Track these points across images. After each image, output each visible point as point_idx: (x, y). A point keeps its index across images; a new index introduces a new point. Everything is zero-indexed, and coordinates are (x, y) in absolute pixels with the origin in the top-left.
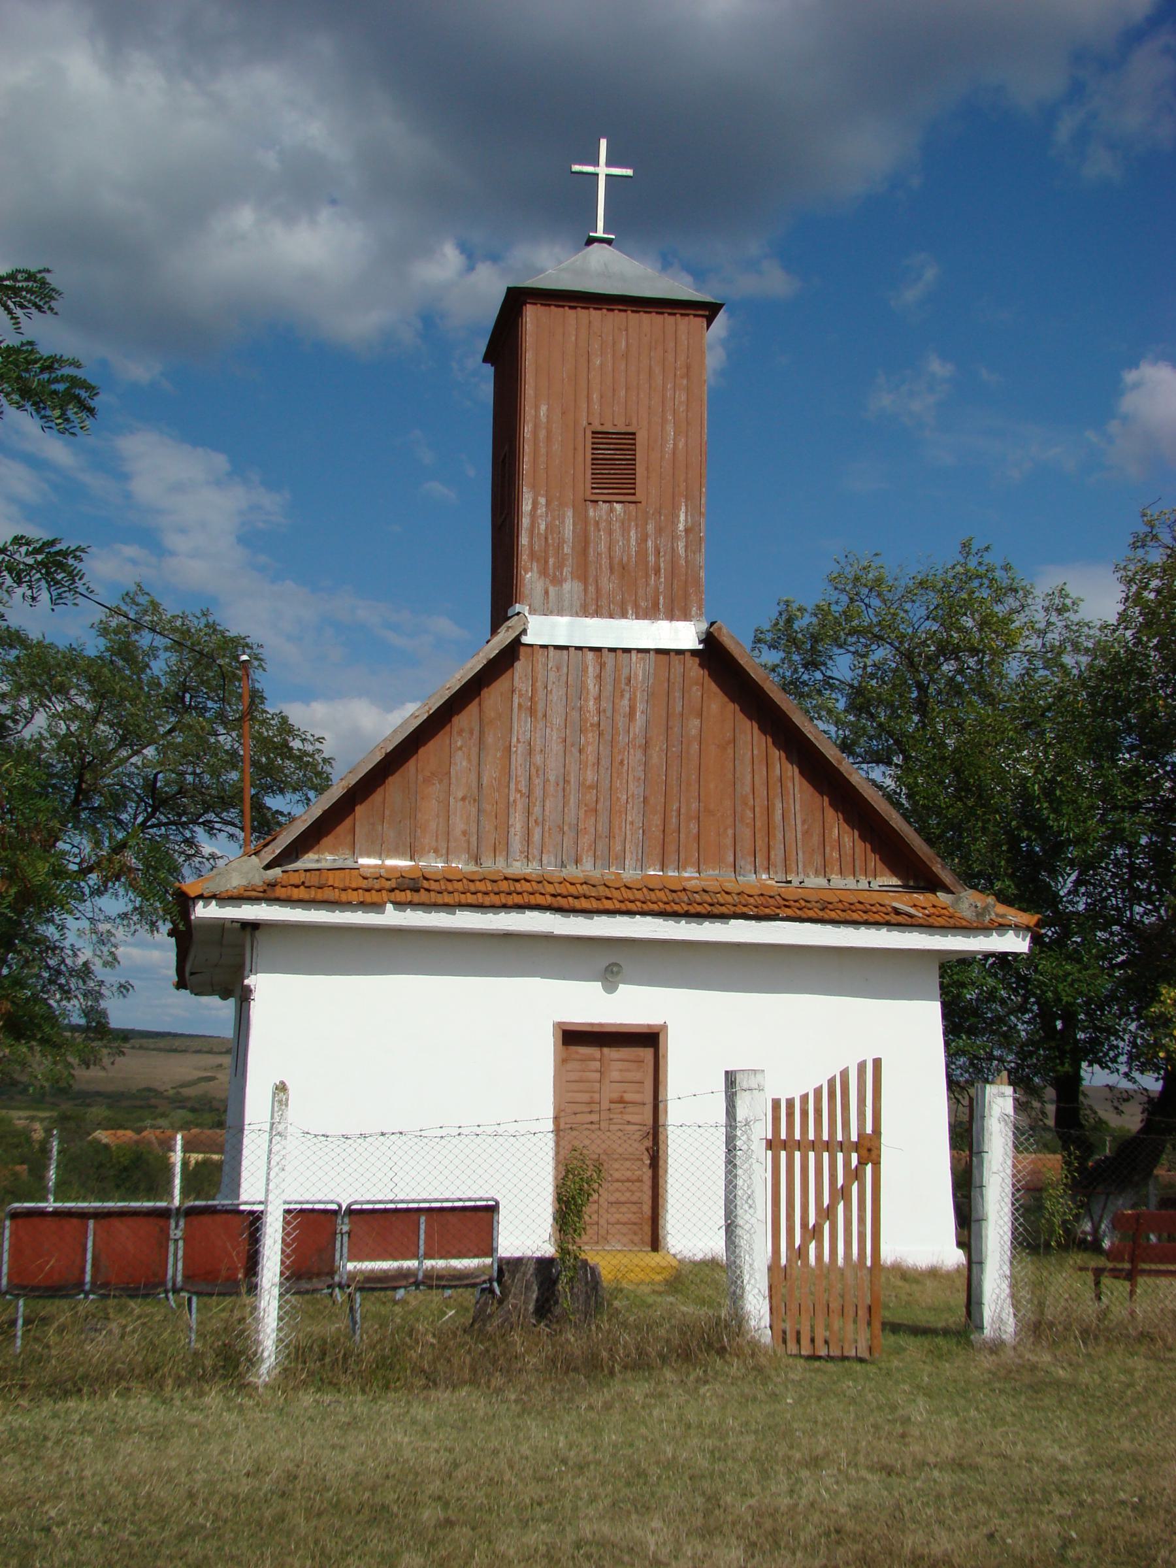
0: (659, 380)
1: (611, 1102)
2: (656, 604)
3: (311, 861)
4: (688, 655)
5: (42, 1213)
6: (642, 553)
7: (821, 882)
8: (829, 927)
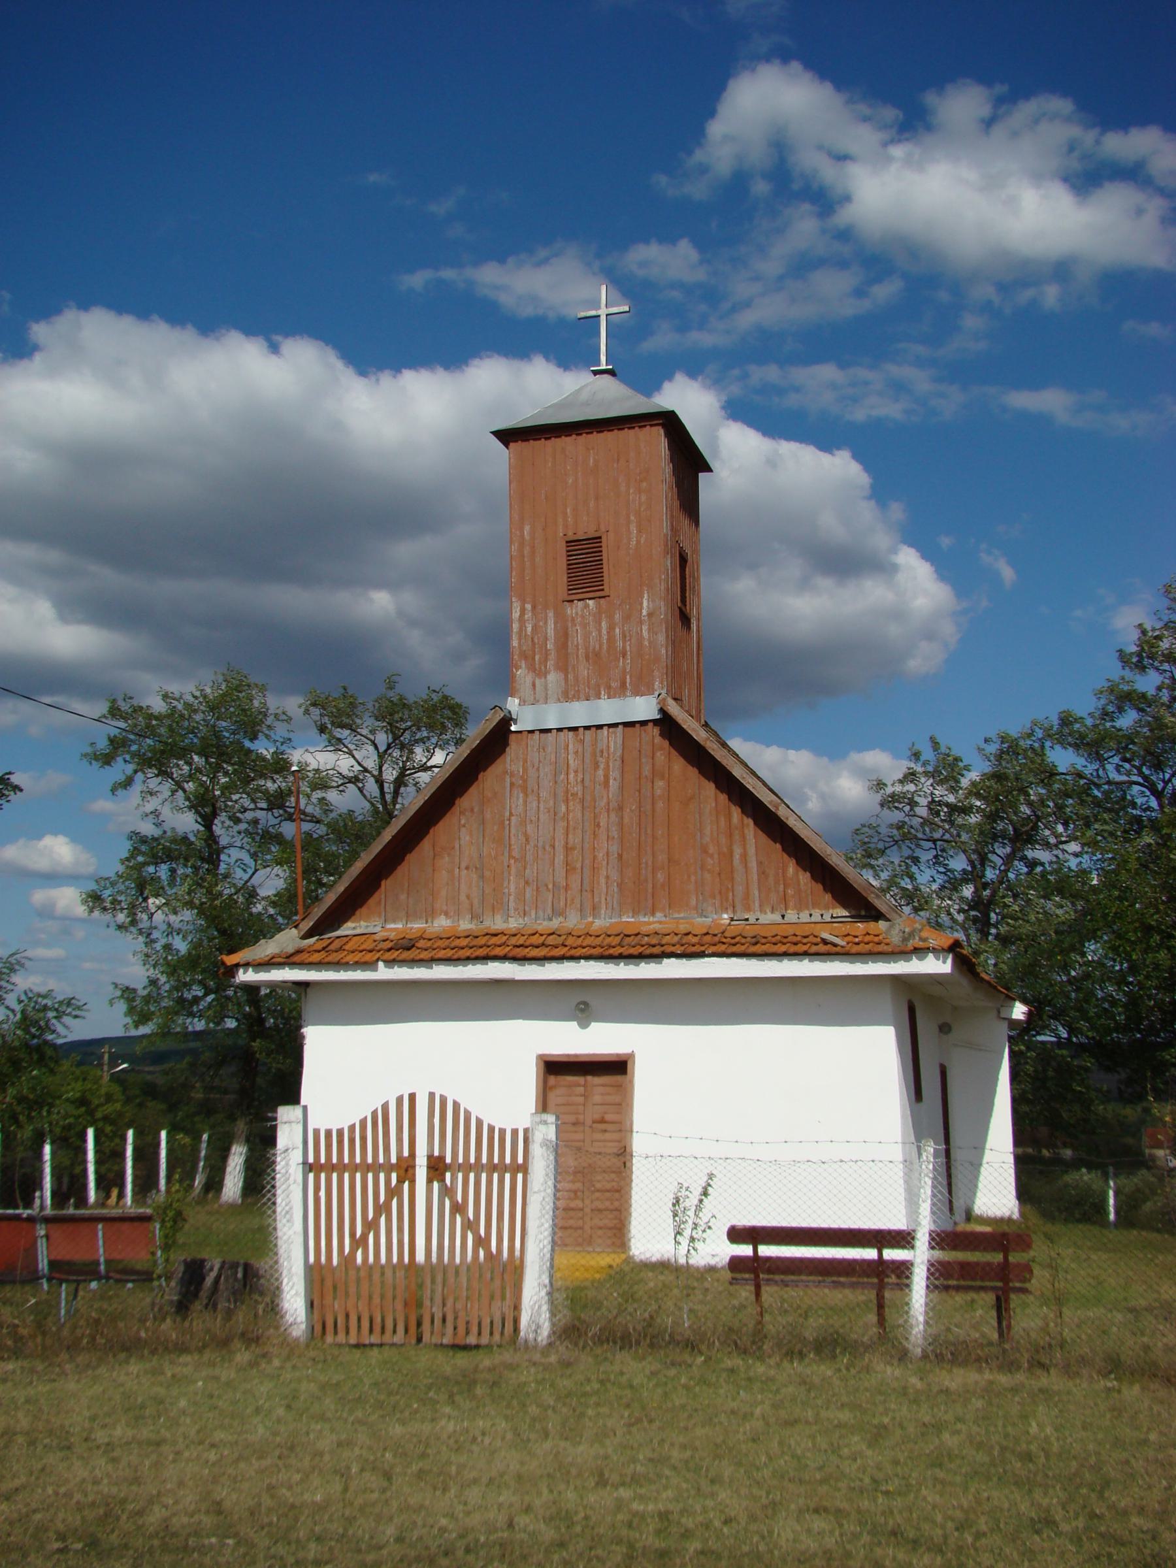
0: (623, 489)
1: (594, 1122)
2: (623, 684)
3: (349, 929)
4: (651, 724)
5: (18, 1217)
6: (611, 639)
7: (776, 917)
8: (734, 959)
